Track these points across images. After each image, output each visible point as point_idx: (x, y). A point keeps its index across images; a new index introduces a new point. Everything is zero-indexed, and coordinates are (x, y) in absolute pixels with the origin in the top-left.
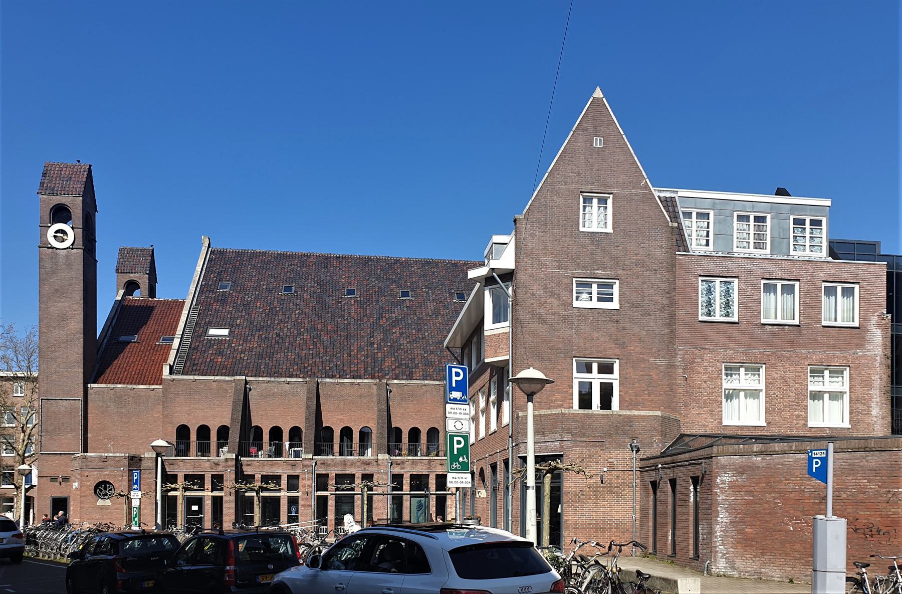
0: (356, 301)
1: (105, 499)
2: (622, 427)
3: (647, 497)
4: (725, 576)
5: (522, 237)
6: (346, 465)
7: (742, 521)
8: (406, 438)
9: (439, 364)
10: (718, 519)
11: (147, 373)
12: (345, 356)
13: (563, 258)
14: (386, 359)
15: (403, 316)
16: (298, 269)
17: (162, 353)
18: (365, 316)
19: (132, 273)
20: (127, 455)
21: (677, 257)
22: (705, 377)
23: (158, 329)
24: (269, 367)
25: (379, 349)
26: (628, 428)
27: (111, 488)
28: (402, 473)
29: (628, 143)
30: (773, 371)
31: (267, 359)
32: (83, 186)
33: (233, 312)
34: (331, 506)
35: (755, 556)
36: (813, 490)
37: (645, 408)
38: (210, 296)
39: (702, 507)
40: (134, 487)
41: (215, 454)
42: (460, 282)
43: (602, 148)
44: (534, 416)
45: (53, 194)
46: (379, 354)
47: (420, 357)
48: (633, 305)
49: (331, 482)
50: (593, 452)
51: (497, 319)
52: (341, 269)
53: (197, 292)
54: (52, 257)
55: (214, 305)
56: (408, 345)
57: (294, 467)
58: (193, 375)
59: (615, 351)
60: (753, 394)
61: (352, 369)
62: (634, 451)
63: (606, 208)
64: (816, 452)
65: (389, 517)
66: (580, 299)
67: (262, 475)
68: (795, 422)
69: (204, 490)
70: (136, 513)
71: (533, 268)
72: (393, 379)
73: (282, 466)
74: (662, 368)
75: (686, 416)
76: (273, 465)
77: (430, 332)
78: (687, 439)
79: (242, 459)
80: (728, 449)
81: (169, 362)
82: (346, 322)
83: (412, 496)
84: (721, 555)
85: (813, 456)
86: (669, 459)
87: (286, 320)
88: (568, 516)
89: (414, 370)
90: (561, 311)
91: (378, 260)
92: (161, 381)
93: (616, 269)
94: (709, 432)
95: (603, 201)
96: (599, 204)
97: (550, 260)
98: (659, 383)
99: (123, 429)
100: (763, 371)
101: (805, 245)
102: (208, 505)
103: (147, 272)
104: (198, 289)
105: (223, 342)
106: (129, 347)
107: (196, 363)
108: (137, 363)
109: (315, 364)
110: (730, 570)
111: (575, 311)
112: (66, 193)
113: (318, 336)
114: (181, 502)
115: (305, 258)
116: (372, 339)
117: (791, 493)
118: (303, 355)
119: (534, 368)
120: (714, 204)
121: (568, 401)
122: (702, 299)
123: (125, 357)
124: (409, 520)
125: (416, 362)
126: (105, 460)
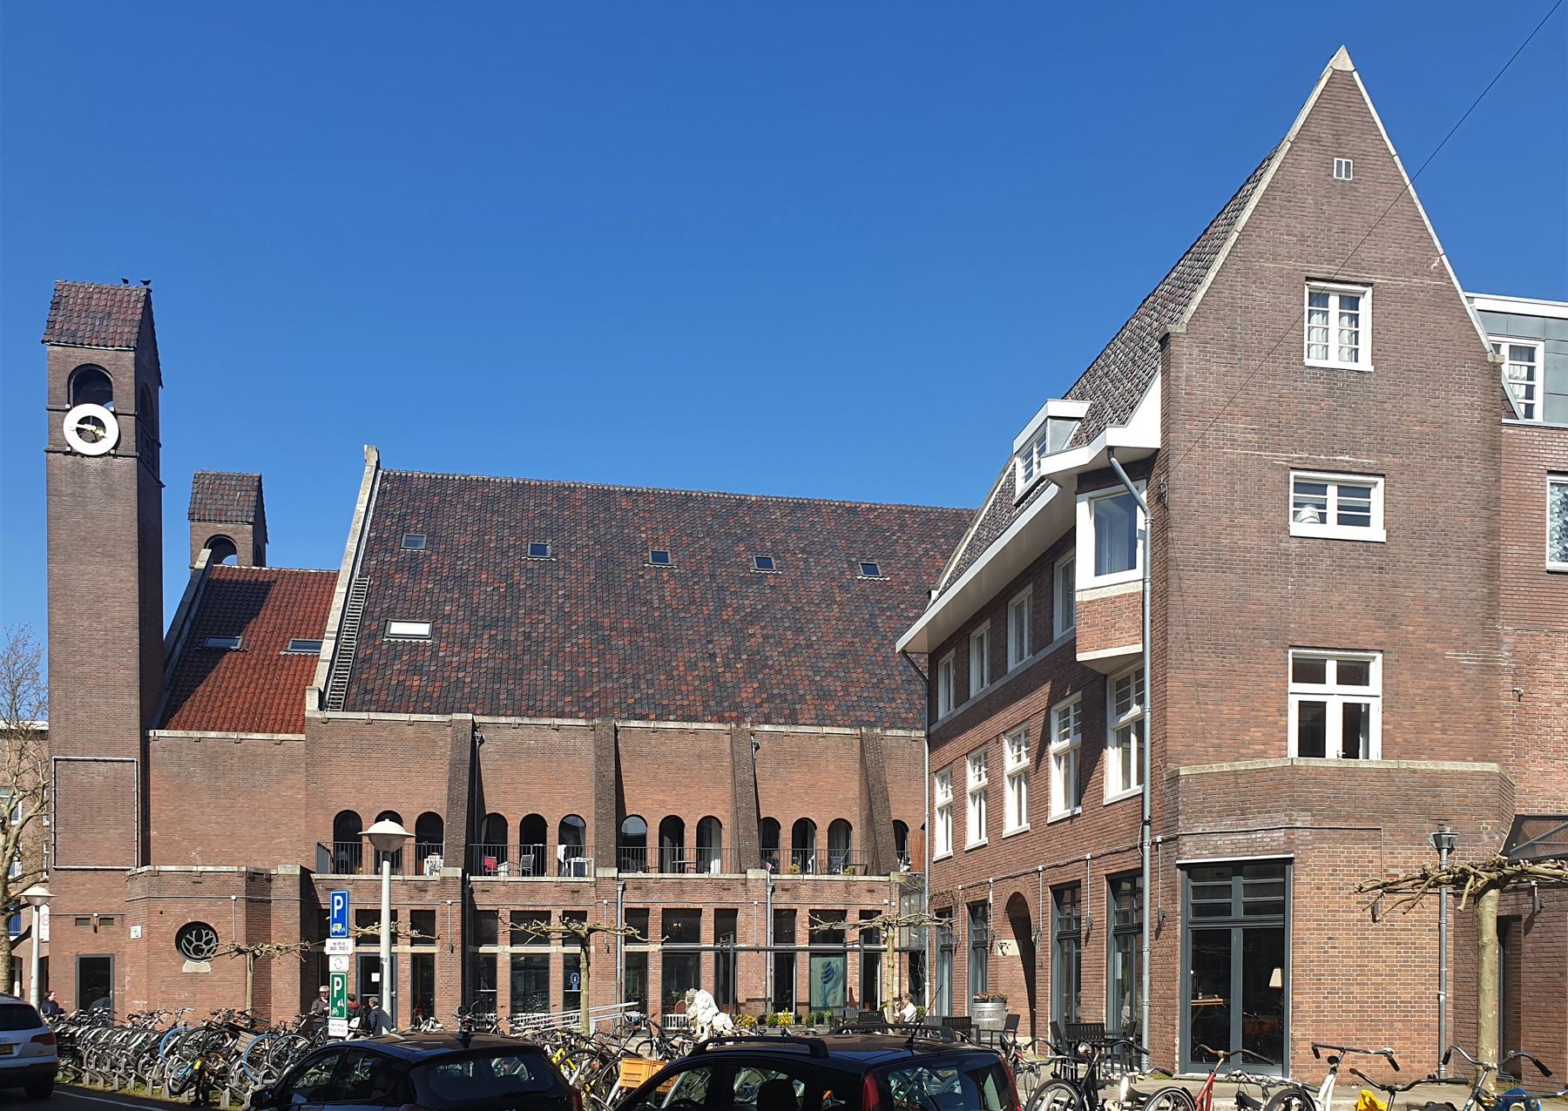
0: (671, 575)
2: (1418, 798)
5: (1183, 376)
6: (683, 892)
8: (788, 838)
9: (844, 695)
11: (266, 711)
12: (662, 677)
13: (1270, 426)
14: (742, 685)
15: (764, 604)
16: (555, 513)
17: (292, 672)
18: (693, 602)
19: (221, 521)
20: (244, 869)
21: (1503, 431)
23: (281, 624)
24: (516, 698)
25: (727, 666)
26: (1429, 799)
27: (210, 937)
28: (794, 907)
31: (510, 682)
32: (136, 330)
33: (436, 591)
34: (655, 974)
38: (386, 559)
40: (333, 929)
41: (413, 870)
42: (865, 543)
43: (1351, 182)
45: (74, 343)
46: (728, 675)
47: (806, 683)
48: (1415, 533)
49: (655, 924)
50: (1355, 853)
53: (362, 553)
54: (73, 473)
55: (397, 576)
56: (782, 658)
57: (576, 895)
58: (366, 711)
59: (1376, 634)
61: (678, 703)
62: (1445, 851)
65: (769, 996)
70: (339, 988)
71: (1204, 447)
74: (1471, 672)
77: (820, 634)
79: (472, 878)
81: (315, 684)
82: (656, 614)
83: (814, 954)
87: (541, 608)
88: (1302, 994)
89: (798, 707)
90: (1264, 545)
91: (706, 499)
93: (1379, 451)
97: (1240, 428)
98: (1465, 704)
99: (221, 820)
103: (251, 520)
104: (363, 547)
105: (420, 649)
106: (226, 659)
107: (369, 687)
108: (244, 690)
111: (1294, 544)
112: (102, 342)
113: (605, 640)
115: (566, 493)
116: (710, 646)
118: (581, 675)
121: (1276, 743)
123: (220, 679)
124: (808, 1001)
125: (801, 692)
126: (198, 880)
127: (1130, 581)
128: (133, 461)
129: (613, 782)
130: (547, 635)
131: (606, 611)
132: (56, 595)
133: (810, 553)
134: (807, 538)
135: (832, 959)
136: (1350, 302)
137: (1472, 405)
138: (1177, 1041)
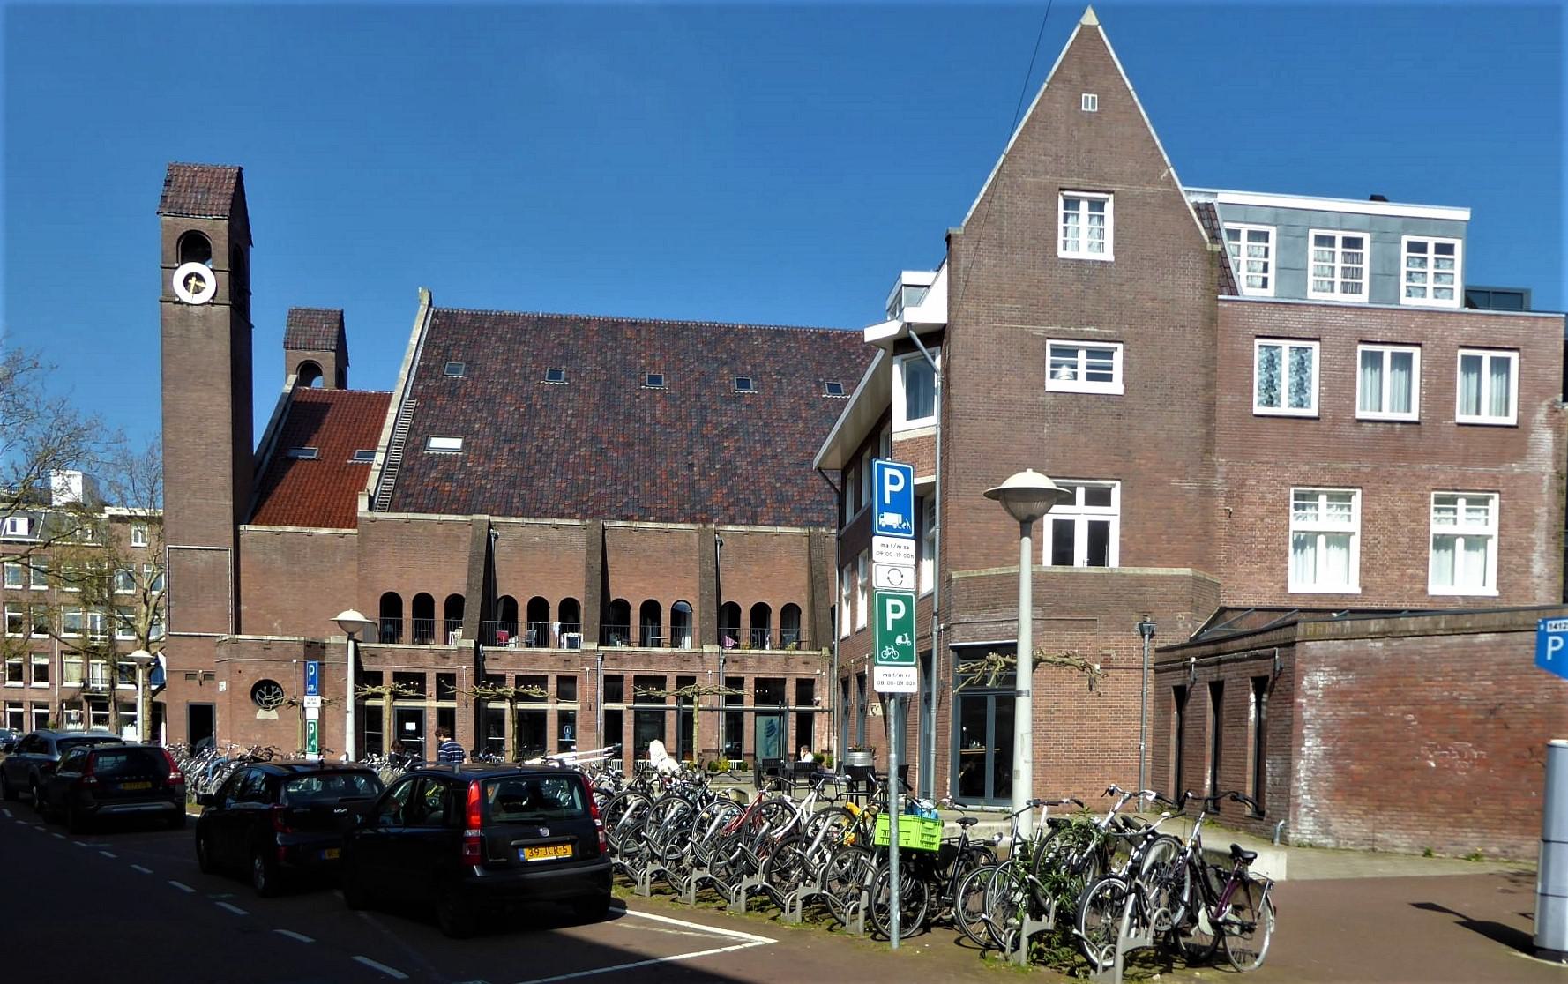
0: (664, 395)
1: (267, 709)
3: (1168, 713)
4: (1311, 846)
6: (651, 662)
7: (1346, 753)
10: (1303, 749)
19: (309, 349)
20: (303, 639)
22: (1261, 511)
25: (703, 474)
29: (1139, 105)
30: (1374, 501)
35: (1366, 813)
36: (1474, 698)
37: (1162, 563)
39: (1272, 728)
42: (833, 365)
44: (1018, 562)
49: (628, 688)
51: (913, 413)
52: (638, 342)
53: (412, 379)
60: (1339, 539)
62: (1147, 636)
63: (1101, 219)
64: (1554, 623)
66: (1057, 375)
67: (517, 676)
68: (1408, 586)
69: (424, 698)
72: (725, 524)
73: (548, 661)
75: (1229, 578)
76: (534, 659)
78: (1230, 616)
79: (485, 648)
80: (1324, 628)
83: (758, 713)
84: (1305, 810)
85: (1549, 630)
86: (1210, 649)
89: (759, 509)
91: (699, 328)
92: (356, 521)
93: (1118, 323)
94: (1266, 603)
95: (1097, 205)
96: (1090, 210)
100: (1356, 501)
101: (1425, 288)
102: (431, 721)
103: (333, 348)
104: (413, 374)
107: (410, 492)
108: (317, 492)
109: (598, 499)
110: (1321, 836)
111: (1049, 398)
113: (603, 452)
114: (387, 716)
116: (690, 457)
117: (1434, 703)
119: (1034, 471)
120: (1277, 215)
122: (1258, 377)
125: (763, 497)
127: (928, 425)
128: (227, 308)
129: (599, 568)
130: (556, 448)
131: (605, 428)
132: (169, 416)
133: (784, 375)
134: (783, 361)
135: (774, 718)
136: (1097, 205)
137: (1194, 284)
138: (949, 780)
